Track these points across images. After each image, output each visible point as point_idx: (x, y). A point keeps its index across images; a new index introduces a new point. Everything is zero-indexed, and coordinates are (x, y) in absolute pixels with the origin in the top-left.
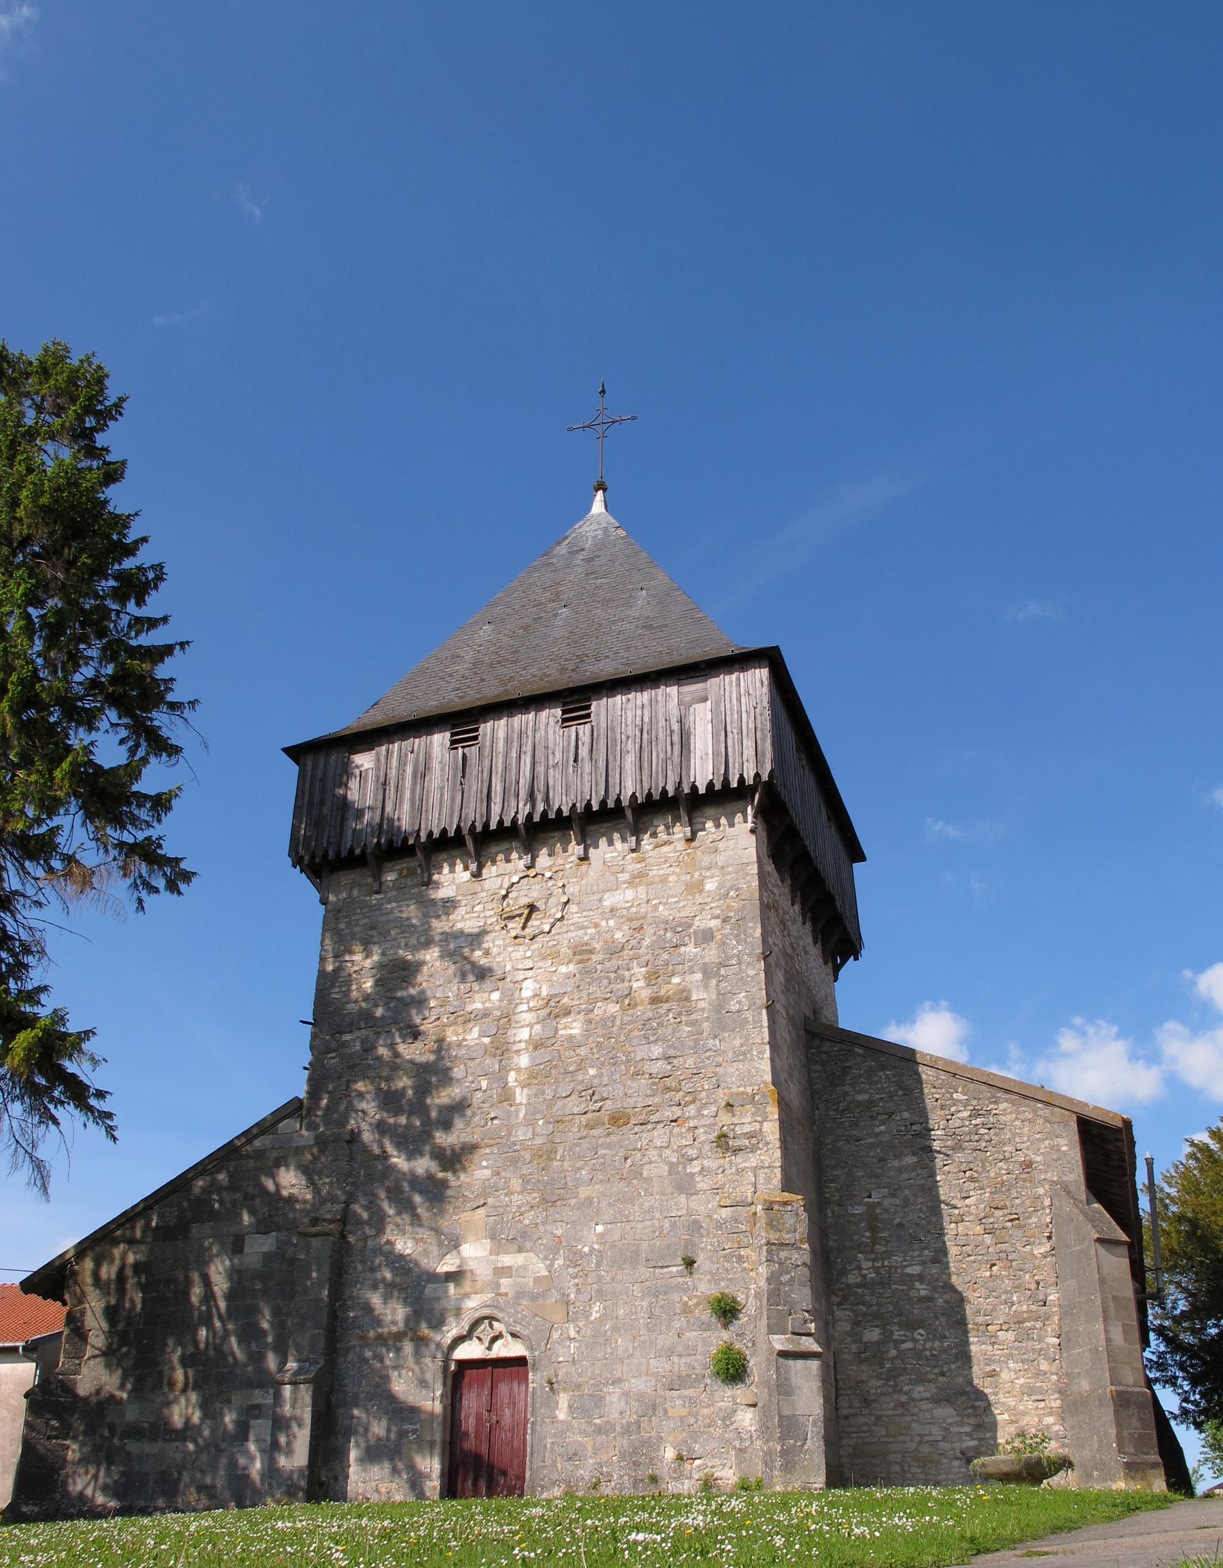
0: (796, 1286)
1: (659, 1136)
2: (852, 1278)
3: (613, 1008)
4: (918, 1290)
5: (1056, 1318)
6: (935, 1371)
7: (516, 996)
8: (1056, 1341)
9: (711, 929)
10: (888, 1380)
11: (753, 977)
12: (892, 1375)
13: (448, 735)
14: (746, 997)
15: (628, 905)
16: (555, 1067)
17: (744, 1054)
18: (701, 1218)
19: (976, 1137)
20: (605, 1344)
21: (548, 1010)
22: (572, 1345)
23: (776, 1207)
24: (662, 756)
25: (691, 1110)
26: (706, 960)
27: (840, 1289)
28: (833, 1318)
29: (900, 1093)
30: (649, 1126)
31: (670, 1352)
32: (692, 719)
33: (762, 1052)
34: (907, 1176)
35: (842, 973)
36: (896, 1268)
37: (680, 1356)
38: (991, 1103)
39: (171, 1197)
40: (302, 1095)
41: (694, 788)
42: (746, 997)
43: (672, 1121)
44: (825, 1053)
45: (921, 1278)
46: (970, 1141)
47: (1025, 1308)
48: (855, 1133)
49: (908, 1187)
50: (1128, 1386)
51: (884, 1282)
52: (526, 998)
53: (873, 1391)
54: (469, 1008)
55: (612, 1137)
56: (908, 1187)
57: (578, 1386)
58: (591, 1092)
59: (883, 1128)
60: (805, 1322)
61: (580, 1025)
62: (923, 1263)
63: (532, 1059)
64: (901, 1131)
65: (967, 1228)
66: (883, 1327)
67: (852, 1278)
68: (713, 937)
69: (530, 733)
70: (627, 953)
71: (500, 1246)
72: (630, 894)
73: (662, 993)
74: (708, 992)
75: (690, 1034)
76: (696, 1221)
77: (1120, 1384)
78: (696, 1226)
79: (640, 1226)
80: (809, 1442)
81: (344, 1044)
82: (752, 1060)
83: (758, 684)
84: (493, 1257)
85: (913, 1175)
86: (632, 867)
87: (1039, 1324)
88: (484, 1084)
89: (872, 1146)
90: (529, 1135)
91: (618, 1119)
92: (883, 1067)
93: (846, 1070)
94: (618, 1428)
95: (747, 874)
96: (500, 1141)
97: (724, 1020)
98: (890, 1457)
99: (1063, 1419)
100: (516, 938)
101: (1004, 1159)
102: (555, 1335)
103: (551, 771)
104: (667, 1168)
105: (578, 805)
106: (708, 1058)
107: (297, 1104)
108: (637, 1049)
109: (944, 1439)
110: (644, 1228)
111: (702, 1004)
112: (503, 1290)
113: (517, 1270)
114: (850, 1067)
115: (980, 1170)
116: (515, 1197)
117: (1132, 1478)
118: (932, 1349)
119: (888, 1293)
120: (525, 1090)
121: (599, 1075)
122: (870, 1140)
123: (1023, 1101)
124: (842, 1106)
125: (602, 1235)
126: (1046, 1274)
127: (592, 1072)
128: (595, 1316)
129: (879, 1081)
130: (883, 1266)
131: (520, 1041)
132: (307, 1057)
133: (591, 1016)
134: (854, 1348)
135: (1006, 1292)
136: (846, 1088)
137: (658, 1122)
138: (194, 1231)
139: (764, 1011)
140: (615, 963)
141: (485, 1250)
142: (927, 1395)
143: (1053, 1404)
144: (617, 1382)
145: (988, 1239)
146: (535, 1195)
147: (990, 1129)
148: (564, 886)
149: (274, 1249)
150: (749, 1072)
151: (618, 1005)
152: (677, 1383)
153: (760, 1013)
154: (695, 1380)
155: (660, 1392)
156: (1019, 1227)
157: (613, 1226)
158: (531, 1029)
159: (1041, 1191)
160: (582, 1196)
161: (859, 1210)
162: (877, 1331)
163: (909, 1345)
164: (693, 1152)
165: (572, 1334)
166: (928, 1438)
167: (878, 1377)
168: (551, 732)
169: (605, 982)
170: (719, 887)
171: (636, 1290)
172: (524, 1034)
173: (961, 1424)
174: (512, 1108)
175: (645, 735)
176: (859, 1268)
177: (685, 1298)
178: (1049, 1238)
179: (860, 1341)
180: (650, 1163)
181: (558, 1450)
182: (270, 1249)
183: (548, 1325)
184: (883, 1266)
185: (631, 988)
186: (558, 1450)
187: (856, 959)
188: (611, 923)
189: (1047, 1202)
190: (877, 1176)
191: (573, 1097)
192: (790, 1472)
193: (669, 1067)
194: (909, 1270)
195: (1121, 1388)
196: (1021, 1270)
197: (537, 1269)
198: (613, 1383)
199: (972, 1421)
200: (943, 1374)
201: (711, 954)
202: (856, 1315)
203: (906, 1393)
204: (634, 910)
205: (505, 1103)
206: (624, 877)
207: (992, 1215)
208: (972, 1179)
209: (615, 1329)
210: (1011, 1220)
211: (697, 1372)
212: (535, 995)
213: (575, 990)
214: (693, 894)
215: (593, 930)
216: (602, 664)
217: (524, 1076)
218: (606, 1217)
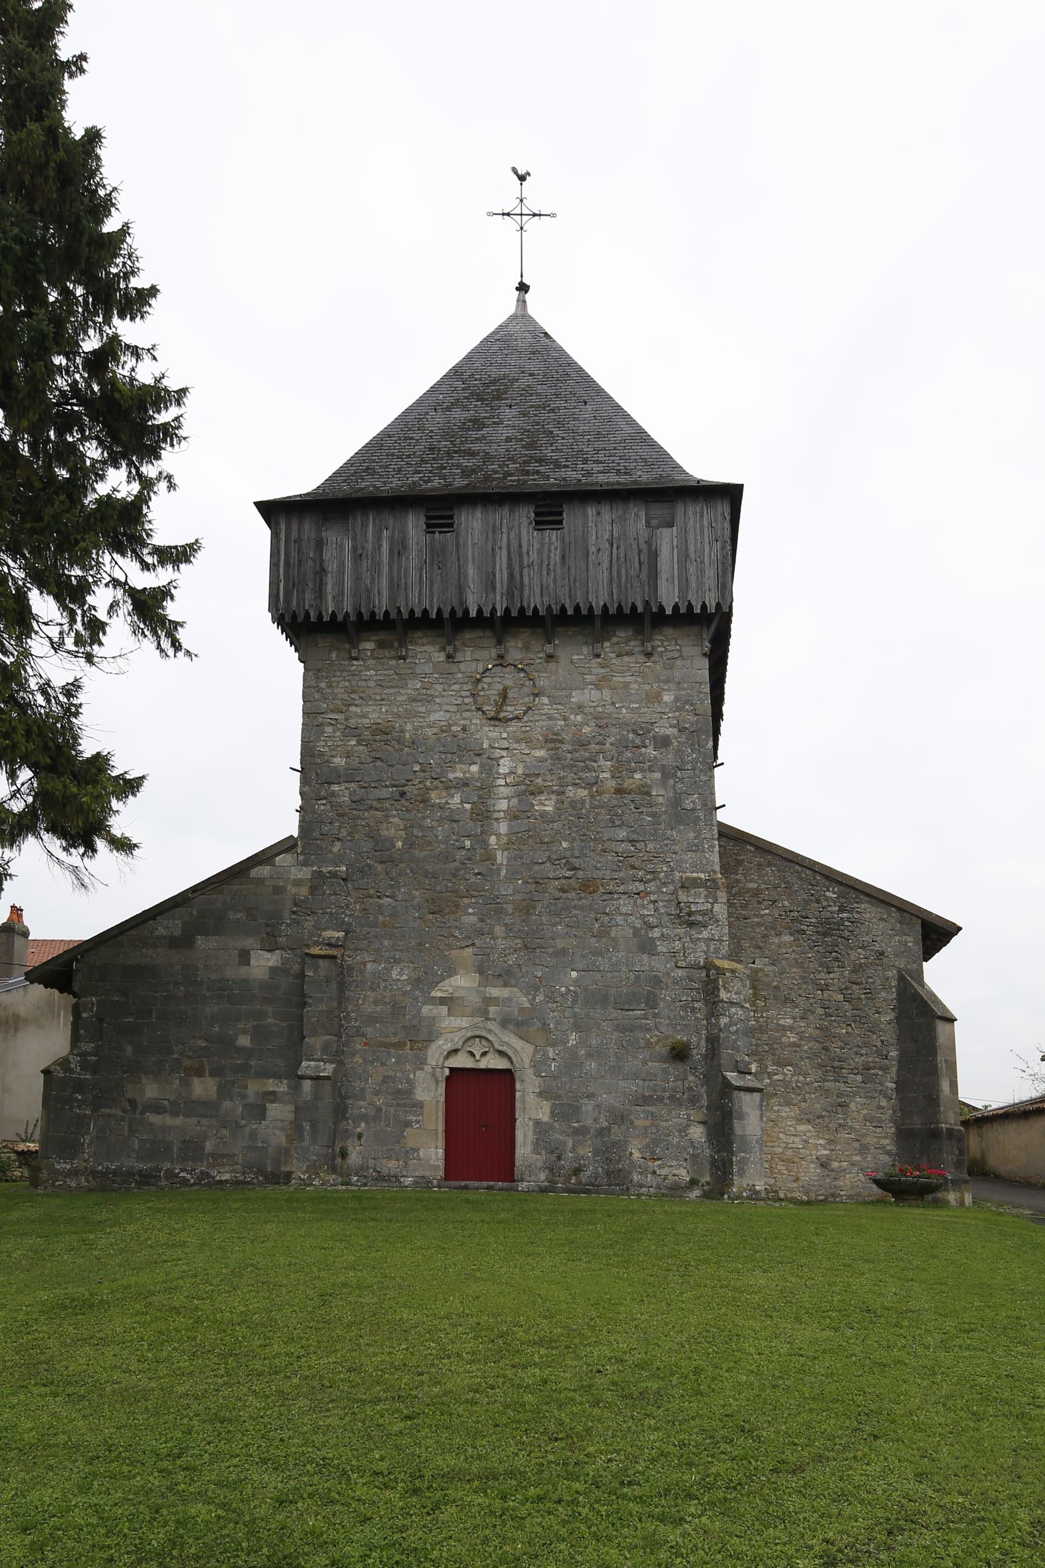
3: (583, 793)
4: (789, 1038)
5: (894, 1070)
7: (494, 771)
9: (668, 736)
11: (705, 782)
15: (594, 704)
18: (661, 974)
20: (581, 1066)
22: (553, 1064)
25: (652, 887)
29: (783, 885)
31: (636, 1076)
37: (644, 1080)
39: (174, 911)
41: (661, 608)
43: (635, 894)
45: (791, 1029)
48: (744, 912)
52: (504, 774)
54: (451, 776)
55: (584, 901)
57: (558, 1097)
59: (767, 911)
61: (553, 803)
62: (794, 1018)
63: (510, 827)
64: (782, 915)
65: (830, 995)
71: (487, 980)
72: (595, 694)
73: (625, 785)
74: (666, 790)
75: (650, 823)
79: (609, 975)
81: (333, 794)
82: (704, 851)
84: (482, 989)
85: (790, 950)
88: (468, 843)
90: (510, 892)
91: (587, 887)
92: (769, 865)
93: (739, 863)
96: (484, 894)
103: (525, 571)
104: (631, 931)
105: (554, 607)
106: (666, 845)
108: (604, 830)
111: (661, 800)
113: (503, 1001)
114: (743, 860)
118: (798, 1081)
119: (765, 1037)
120: (506, 853)
121: (571, 849)
122: (756, 920)
123: (880, 904)
129: (766, 874)
131: (499, 811)
132: (298, 802)
137: (624, 893)
138: (199, 942)
141: (475, 981)
144: (590, 1096)
145: (847, 1005)
147: (852, 922)
149: (279, 964)
150: (701, 861)
151: (586, 791)
156: (869, 998)
157: (586, 973)
158: (509, 801)
159: (889, 974)
166: (792, 1145)
170: (677, 699)
171: (607, 1026)
172: (503, 805)
173: (818, 1137)
174: (494, 867)
177: (648, 1036)
180: (617, 925)
182: (275, 964)
184: (762, 1017)
185: (598, 777)
190: (760, 948)
194: (782, 1022)
197: (521, 1002)
201: (669, 758)
203: (775, 1112)
205: (487, 862)
207: (850, 989)
208: (836, 959)
210: (865, 994)
211: (658, 1094)
213: (548, 773)
215: (563, 722)
216: (563, 473)
217: (505, 840)
218: (580, 966)
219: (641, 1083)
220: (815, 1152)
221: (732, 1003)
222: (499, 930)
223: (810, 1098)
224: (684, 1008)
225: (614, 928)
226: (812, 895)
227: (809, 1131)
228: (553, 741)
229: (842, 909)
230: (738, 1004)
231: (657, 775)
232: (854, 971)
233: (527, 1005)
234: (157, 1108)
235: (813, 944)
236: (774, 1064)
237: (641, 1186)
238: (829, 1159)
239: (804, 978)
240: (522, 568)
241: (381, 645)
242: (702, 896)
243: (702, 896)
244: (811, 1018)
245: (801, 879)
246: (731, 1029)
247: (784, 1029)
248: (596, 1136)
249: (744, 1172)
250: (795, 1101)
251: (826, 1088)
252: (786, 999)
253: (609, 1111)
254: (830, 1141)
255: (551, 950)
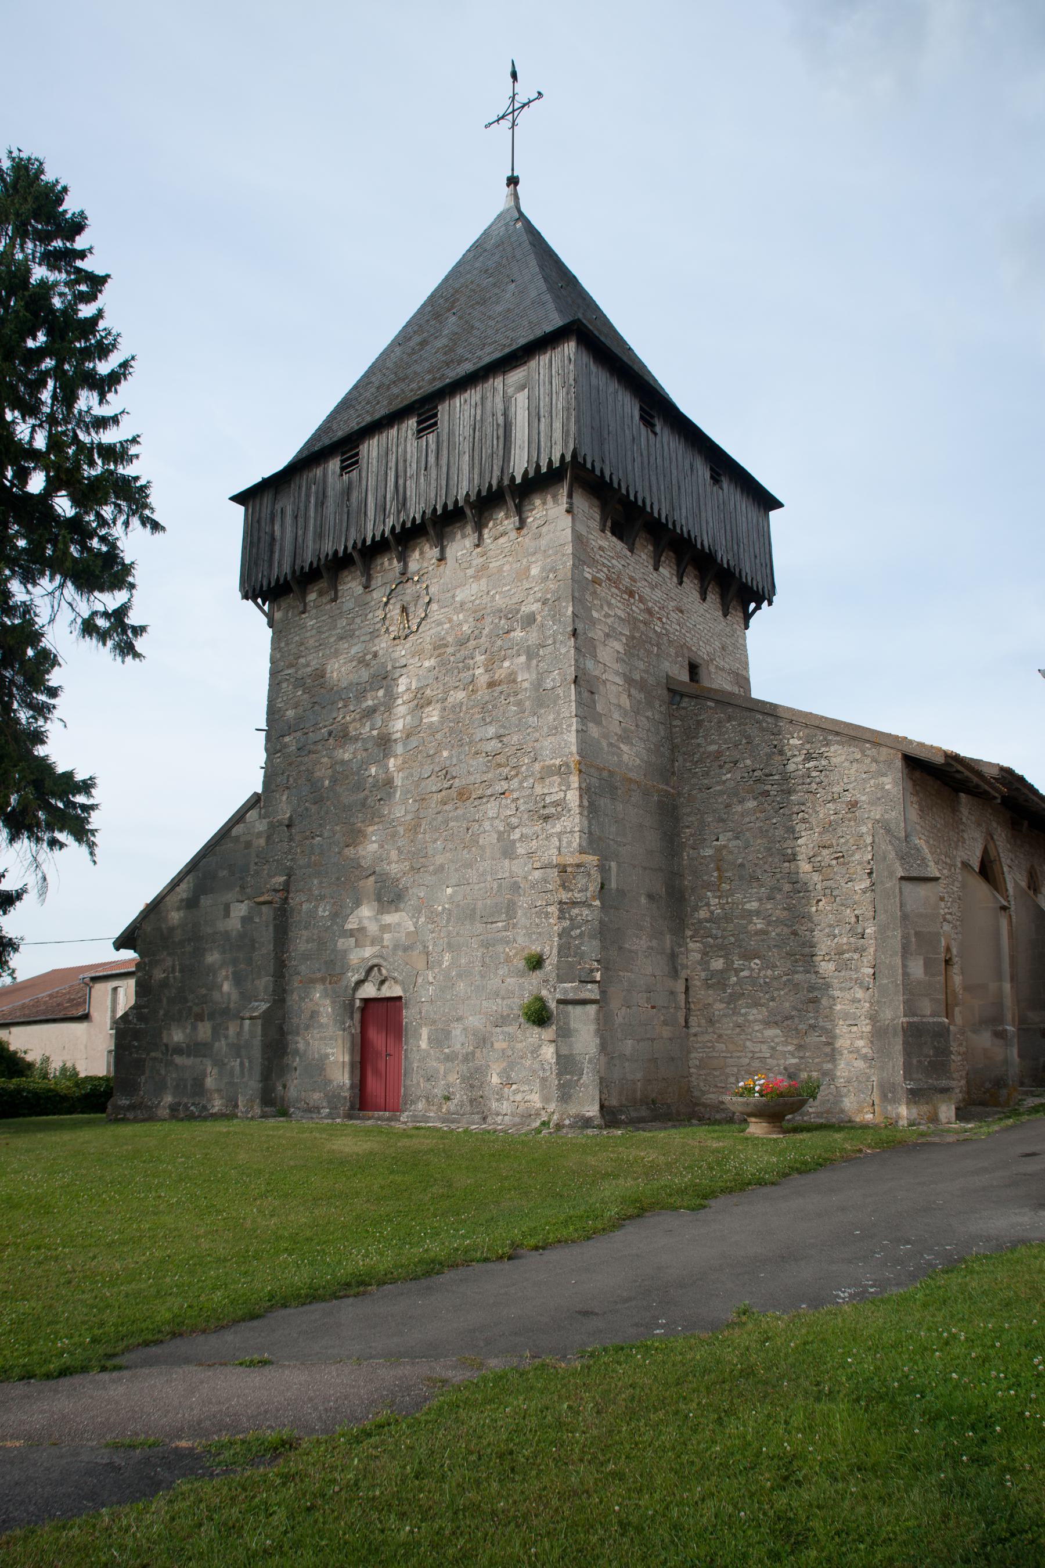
0: (586, 939)
1: (491, 808)
2: (703, 914)
3: (461, 695)
4: (755, 924)
5: (872, 950)
6: (767, 996)
8: (871, 971)
10: (729, 1003)
12: (733, 998)
13: (339, 458)
14: (559, 674)
16: (420, 752)
17: (556, 728)
19: (808, 780)
21: (416, 702)
23: (569, 869)
24: (489, 451)
25: (515, 783)
26: (530, 643)
27: (692, 924)
28: (687, 949)
29: (744, 741)
30: (484, 800)
32: (513, 409)
33: (570, 726)
34: (747, 820)
35: (753, 621)
36: (738, 904)
37: (503, 998)
38: (824, 746)
40: (260, 791)
42: (559, 674)
44: (683, 708)
45: (757, 913)
46: (803, 784)
47: (845, 940)
48: (706, 781)
49: (748, 830)
50: (924, 1016)
51: (727, 918)
53: (717, 1013)
56: (748, 830)
57: (434, 1022)
58: (444, 772)
59: (729, 776)
60: (592, 971)
62: (760, 900)
66: (725, 957)
67: (703, 914)
68: (535, 620)
69: (394, 449)
70: (472, 643)
73: (496, 677)
74: (530, 672)
76: (516, 882)
77: (914, 1015)
78: (515, 887)
79: (477, 887)
80: (585, 1077)
83: (566, 362)
85: (753, 818)
86: (478, 561)
87: (856, 956)
89: (721, 793)
90: (403, 813)
91: (463, 795)
92: (730, 719)
93: (699, 723)
94: (460, 1057)
95: (564, 555)
97: (542, 698)
98: (728, 1070)
99: (872, 1042)
100: (394, 639)
101: (833, 800)
102: (420, 980)
103: (408, 483)
104: (496, 836)
107: (256, 798)
109: (771, 1057)
110: (480, 889)
111: (526, 685)
112: (385, 943)
115: (810, 811)
116: (393, 866)
117: (915, 1103)
118: (766, 977)
119: (731, 927)
121: (450, 757)
122: (718, 788)
124: (697, 757)
125: (451, 896)
126: (864, 909)
127: (445, 754)
128: (446, 964)
130: (727, 903)
133: (446, 704)
134: (703, 974)
135: (830, 926)
136: (699, 741)
137: (491, 796)
139: (573, 686)
140: (464, 653)
142: (760, 1017)
143: (864, 1029)
144: (459, 1019)
146: (406, 863)
148: (427, 587)
152: (501, 1021)
153: (570, 688)
154: (513, 1019)
155: (489, 1028)
156: (844, 864)
160: (438, 863)
161: (708, 852)
162: (721, 961)
163: (745, 973)
164: (514, 821)
165: (431, 979)
167: (721, 1001)
168: (409, 445)
169: (456, 671)
173: (786, 1043)
175: (477, 433)
176: (708, 905)
177: (507, 950)
178: (870, 874)
179: (708, 970)
181: (422, 1072)
183: (415, 972)
186: (422, 1072)
187: (770, 604)
188: (461, 616)
189: (869, 840)
190: (723, 820)
191: (433, 777)
192: (566, 1102)
193: (500, 745)
194: (747, 906)
195: (915, 1019)
196: (842, 905)
198: (457, 1020)
199: (795, 1042)
200: (773, 999)
201: (533, 637)
202: (705, 947)
203: (742, 1015)
204: (477, 602)
206: (470, 572)
209: (459, 976)
210: (837, 858)
212: (408, 689)
214: (521, 581)
218: (453, 881)
219: (499, 1001)
220: (782, 1061)
221: (574, 903)
222: (394, 855)
223: (779, 996)
224: (538, 914)
225: (482, 836)
226: (775, 746)
227: (777, 1037)
228: (440, 647)
229: (809, 757)
230: (585, 904)
231: (523, 659)
232: (825, 830)
233: (412, 929)
234: (178, 1050)
235: (777, 807)
236: (740, 958)
237: (498, 1114)
238: (798, 1068)
239: (770, 849)
240: (405, 481)
241: (321, 594)
242: (556, 785)
243: (556, 785)
244: (778, 897)
245: (763, 730)
246: (572, 933)
247: (750, 913)
248: (463, 1061)
249: (570, 1097)
250: (763, 1001)
251: (796, 981)
252: (752, 877)
253: (474, 1035)
254: (800, 1047)
255: (431, 868)
